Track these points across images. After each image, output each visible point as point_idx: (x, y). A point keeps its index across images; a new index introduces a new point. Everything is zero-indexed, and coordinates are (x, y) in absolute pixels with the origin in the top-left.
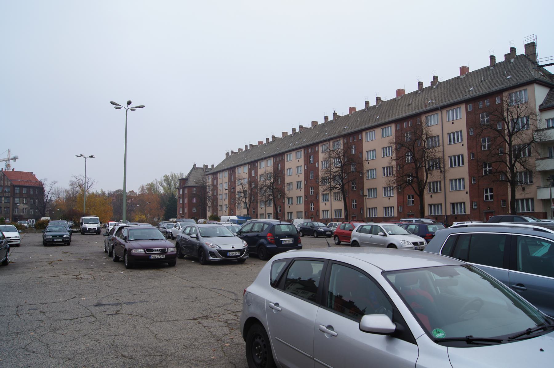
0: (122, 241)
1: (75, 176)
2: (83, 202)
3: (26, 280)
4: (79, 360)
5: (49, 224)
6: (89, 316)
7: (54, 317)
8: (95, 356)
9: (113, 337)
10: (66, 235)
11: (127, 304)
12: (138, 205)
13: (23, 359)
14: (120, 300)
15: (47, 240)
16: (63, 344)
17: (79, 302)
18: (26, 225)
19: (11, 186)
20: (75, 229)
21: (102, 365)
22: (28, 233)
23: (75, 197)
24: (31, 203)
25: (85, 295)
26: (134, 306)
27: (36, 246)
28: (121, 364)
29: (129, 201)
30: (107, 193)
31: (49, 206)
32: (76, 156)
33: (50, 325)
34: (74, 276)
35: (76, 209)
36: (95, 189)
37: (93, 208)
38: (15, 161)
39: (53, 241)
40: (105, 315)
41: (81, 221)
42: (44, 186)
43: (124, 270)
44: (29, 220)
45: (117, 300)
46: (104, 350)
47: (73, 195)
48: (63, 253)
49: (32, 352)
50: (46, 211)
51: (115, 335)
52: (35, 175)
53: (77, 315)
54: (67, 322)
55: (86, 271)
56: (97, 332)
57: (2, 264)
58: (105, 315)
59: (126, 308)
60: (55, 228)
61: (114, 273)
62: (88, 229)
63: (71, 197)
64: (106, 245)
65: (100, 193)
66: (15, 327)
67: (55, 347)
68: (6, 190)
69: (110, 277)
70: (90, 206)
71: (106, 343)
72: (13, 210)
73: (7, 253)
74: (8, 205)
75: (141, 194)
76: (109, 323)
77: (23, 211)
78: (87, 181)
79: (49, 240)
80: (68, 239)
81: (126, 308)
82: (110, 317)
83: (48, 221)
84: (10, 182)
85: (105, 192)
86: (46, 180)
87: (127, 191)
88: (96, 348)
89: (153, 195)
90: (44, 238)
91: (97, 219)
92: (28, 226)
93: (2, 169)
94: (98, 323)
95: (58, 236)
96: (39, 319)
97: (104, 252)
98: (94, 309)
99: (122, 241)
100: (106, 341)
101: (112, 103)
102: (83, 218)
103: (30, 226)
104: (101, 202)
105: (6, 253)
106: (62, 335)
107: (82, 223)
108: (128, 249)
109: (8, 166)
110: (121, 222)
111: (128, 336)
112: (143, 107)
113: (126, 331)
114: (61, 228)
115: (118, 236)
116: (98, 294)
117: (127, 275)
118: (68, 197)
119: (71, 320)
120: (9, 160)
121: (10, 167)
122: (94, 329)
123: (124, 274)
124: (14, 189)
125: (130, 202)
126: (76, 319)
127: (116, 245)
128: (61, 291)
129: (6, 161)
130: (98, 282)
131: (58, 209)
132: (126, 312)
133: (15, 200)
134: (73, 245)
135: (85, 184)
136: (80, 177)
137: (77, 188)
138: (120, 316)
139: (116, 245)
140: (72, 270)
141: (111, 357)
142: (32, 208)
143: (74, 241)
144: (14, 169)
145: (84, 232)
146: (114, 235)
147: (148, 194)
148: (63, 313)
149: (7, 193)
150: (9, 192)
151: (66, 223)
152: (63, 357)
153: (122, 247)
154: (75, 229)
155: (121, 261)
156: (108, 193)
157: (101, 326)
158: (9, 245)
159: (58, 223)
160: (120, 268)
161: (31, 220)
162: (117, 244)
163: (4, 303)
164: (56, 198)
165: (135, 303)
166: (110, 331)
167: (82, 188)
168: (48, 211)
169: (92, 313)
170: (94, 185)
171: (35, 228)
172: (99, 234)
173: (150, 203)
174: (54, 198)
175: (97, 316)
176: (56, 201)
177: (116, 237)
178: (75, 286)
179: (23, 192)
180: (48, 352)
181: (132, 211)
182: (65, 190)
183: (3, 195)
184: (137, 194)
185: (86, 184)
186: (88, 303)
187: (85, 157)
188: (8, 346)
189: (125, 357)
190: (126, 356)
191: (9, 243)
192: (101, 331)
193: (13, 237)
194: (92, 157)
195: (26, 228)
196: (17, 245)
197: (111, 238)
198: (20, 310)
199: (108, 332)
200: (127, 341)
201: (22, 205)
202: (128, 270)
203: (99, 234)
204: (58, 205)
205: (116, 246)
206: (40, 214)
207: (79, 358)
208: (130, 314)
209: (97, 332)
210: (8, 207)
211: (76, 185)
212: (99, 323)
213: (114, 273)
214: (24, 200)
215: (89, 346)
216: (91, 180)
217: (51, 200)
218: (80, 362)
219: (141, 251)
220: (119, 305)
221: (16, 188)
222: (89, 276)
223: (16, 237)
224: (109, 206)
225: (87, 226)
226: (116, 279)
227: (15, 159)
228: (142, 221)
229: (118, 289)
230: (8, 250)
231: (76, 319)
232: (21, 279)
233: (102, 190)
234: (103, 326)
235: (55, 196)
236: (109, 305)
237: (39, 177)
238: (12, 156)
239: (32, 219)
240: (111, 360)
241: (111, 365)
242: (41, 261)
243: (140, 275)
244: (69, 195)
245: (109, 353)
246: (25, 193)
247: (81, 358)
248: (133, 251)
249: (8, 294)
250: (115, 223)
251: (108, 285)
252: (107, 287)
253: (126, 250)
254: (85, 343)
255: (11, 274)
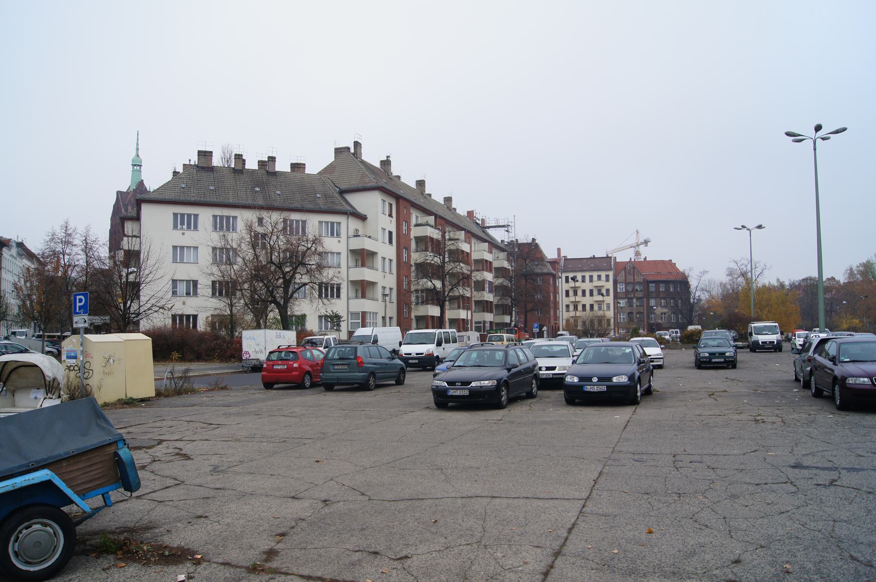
0: (829, 364)
1: (734, 261)
2: (750, 300)
3: (680, 418)
4: (778, 552)
5: (703, 336)
6: (785, 483)
7: (730, 477)
8: (804, 549)
9: (831, 523)
10: (730, 352)
11: (850, 470)
12: (844, 302)
13: (693, 534)
14: (835, 462)
15: (701, 360)
16: (748, 522)
17: (765, 459)
18: (667, 337)
19: (644, 281)
20: (740, 344)
21: (818, 567)
22: (672, 349)
23: (737, 293)
24: (672, 305)
25: (773, 448)
26: (862, 475)
27: (686, 368)
28: (852, 571)
29: (827, 296)
30: (787, 283)
31: (698, 309)
32: (735, 228)
33: (724, 488)
34: (751, 417)
35: (739, 312)
36: (768, 278)
37: (767, 308)
38: (646, 245)
39: (710, 362)
40: (811, 484)
41: (749, 331)
42: (689, 279)
43: (833, 412)
44: (670, 330)
45: (829, 461)
46: (818, 542)
47: (733, 291)
48: (728, 380)
49: (704, 526)
50: (693, 316)
51: (835, 521)
52: (675, 264)
53: (766, 479)
54: (751, 488)
55: (768, 411)
56: (802, 510)
57: (644, 393)
58: (811, 484)
59: (848, 477)
60: (712, 341)
61: (817, 417)
62: (761, 344)
63: (729, 294)
64: (798, 369)
65: (776, 284)
66: (675, 485)
67: (737, 524)
68: (637, 287)
69: (812, 422)
70: (761, 307)
71: (819, 531)
72: (648, 317)
73: (650, 378)
74: (641, 309)
75: (849, 282)
76: (821, 499)
77: (662, 317)
78: (754, 267)
79: (705, 360)
80: (733, 359)
81: (848, 477)
82: (820, 489)
83: (699, 333)
84: (642, 277)
85: (783, 282)
86: (691, 269)
87: (826, 276)
88: (804, 537)
89: (871, 282)
90: (696, 357)
91: (775, 326)
92: (671, 339)
93: (631, 259)
94: (801, 496)
95: (717, 355)
96: (707, 478)
97: (792, 381)
98: (793, 474)
99: (829, 364)
100: (820, 528)
101: (789, 134)
102: (753, 325)
103: (673, 338)
104: (778, 300)
105: (649, 377)
106: (746, 506)
107: (751, 334)
108: (839, 377)
109: (638, 254)
110: (815, 331)
111: (859, 526)
112: (844, 130)
113: (854, 517)
114: (721, 341)
115: (820, 355)
116: (795, 448)
117: (842, 421)
118: (725, 294)
119: (757, 485)
120: (638, 245)
121: (640, 255)
122: (796, 505)
123: (836, 420)
124: (648, 287)
125: (828, 297)
126: (765, 484)
127: (816, 369)
128: (734, 438)
129: (634, 247)
130: (791, 428)
131: (712, 313)
132: (850, 484)
133: (650, 301)
134: (741, 368)
135: (751, 271)
136: (743, 262)
137: (739, 279)
138: (839, 489)
139: (816, 369)
140: (746, 406)
141: (832, 556)
142: (674, 313)
143: (742, 362)
144: (646, 257)
145: (756, 347)
146: (811, 353)
147: (862, 281)
148: (742, 473)
149: (639, 292)
150: (641, 291)
151: (727, 333)
152: (752, 542)
153: (826, 372)
154: (741, 343)
155: (826, 398)
156: (790, 284)
157: (808, 501)
158: (652, 365)
159: (716, 334)
160: (825, 408)
161: (674, 330)
162: (817, 368)
163: (656, 448)
164: (707, 297)
165: (863, 470)
166: (824, 512)
167: (747, 280)
168: (697, 317)
169: (789, 479)
170: (766, 272)
171: (681, 341)
172: (780, 350)
173: (866, 297)
174: (704, 297)
175: (797, 483)
176: (708, 301)
177: (816, 356)
178: (754, 432)
179: (661, 290)
180: (728, 530)
181: (833, 313)
182: (721, 284)
183: (634, 295)
184: (842, 282)
185: (753, 272)
186: (780, 462)
187: (748, 229)
188: (669, 511)
189: (858, 561)
190: (860, 560)
191: (652, 364)
192: (808, 509)
193: (654, 355)
194: (760, 227)
195: (668, 341)
196: (660, 367)
197: (806, 358)
198: (678, 461)
199: (821, 513)
200: (858, 533)
201: (659, 308)
202: (842, 413)
203: (780, 350)
204: (711, 306)
205: (816, 372)
206: (685, 321)
207: (777, 547)
208: (857, 489)
209: (802, 510)
210: (642, 313)
211: (737, 275)
212: (803, 497)
213: (817, 417)
214: (663, 301)
215: (790, 531)
216: (761, 264)
217: (699, 300)
218: (780, 555)
219: (863, 381)
220: (835, 470)
221: (650, 285)
222: (774, 419)
223: (658, 355)
224: (794, 305)
225: (759, 339)
226: (821, 426)
227: (646, 242)
228: (856, 330)
229: (829, 443)
230: (652, 374)
231: (765, 484)
232: (673, 416)
233: (778, 280)
234: (812, 503)
235: (705, 293)
236: (817, 468)
237: (681, 267)
238: (642, 240)
239: (674, 329)
240: (833, 562)
241: (834, 569)
242: (697, 390)
243: (864, 423)
244: (727, 291)
245: (827, 548)
246: (662, 291)
247: (780, 549)
248: (849, 380)
249: (659, 436)
250: (807, 334)
251: (809, 435)
252: (808, 438)
253: (835, 378)
254: (784, 526)
255: (658, 407)
